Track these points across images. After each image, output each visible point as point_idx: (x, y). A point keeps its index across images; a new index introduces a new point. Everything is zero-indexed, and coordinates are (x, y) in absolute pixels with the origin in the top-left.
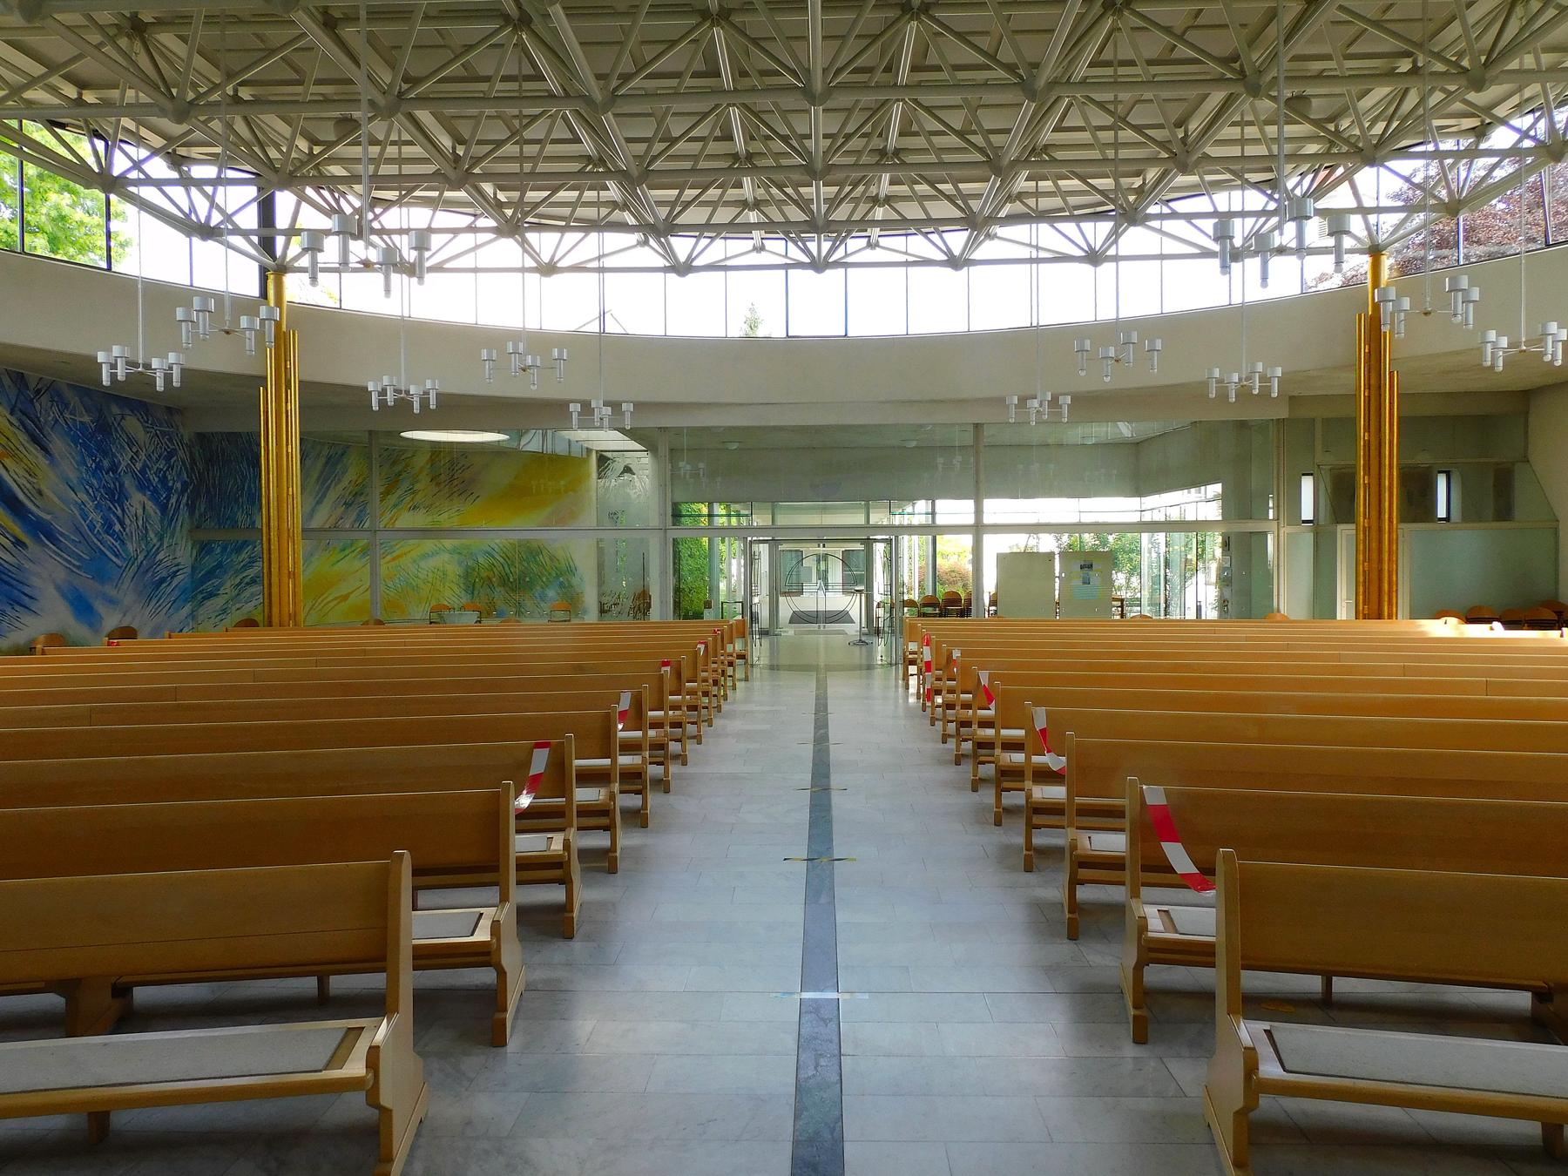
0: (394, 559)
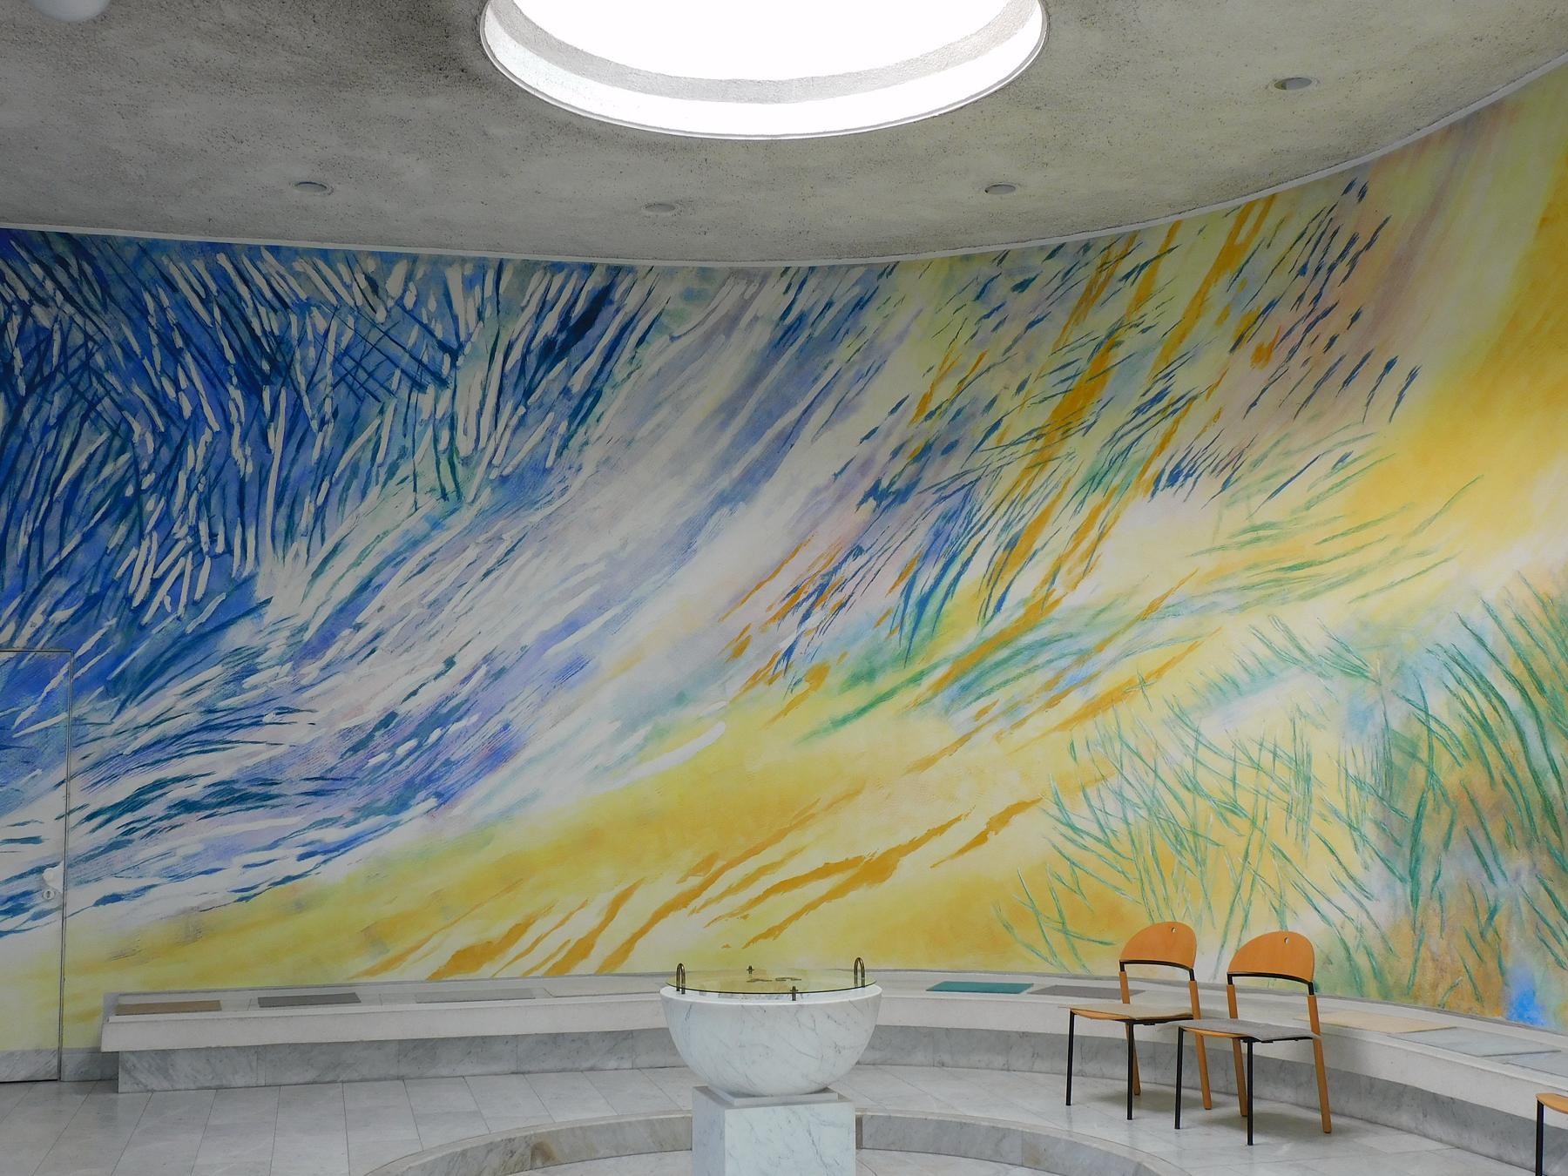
0: (1094, 708)
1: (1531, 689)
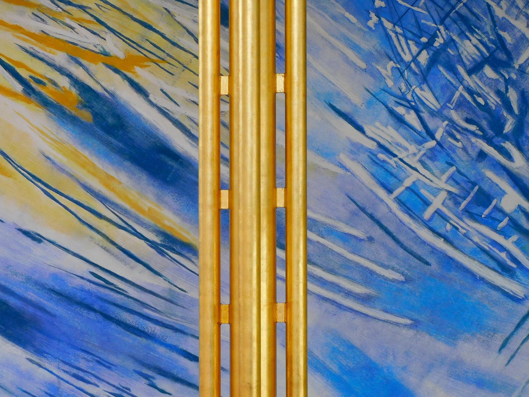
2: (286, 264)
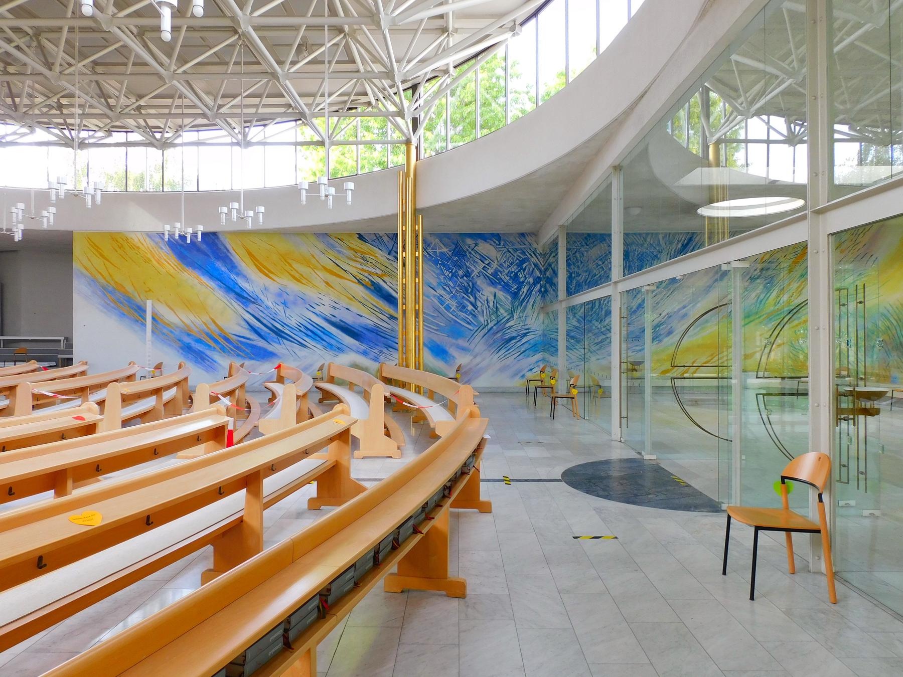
1: (899, 321)
2: (418, 322)
